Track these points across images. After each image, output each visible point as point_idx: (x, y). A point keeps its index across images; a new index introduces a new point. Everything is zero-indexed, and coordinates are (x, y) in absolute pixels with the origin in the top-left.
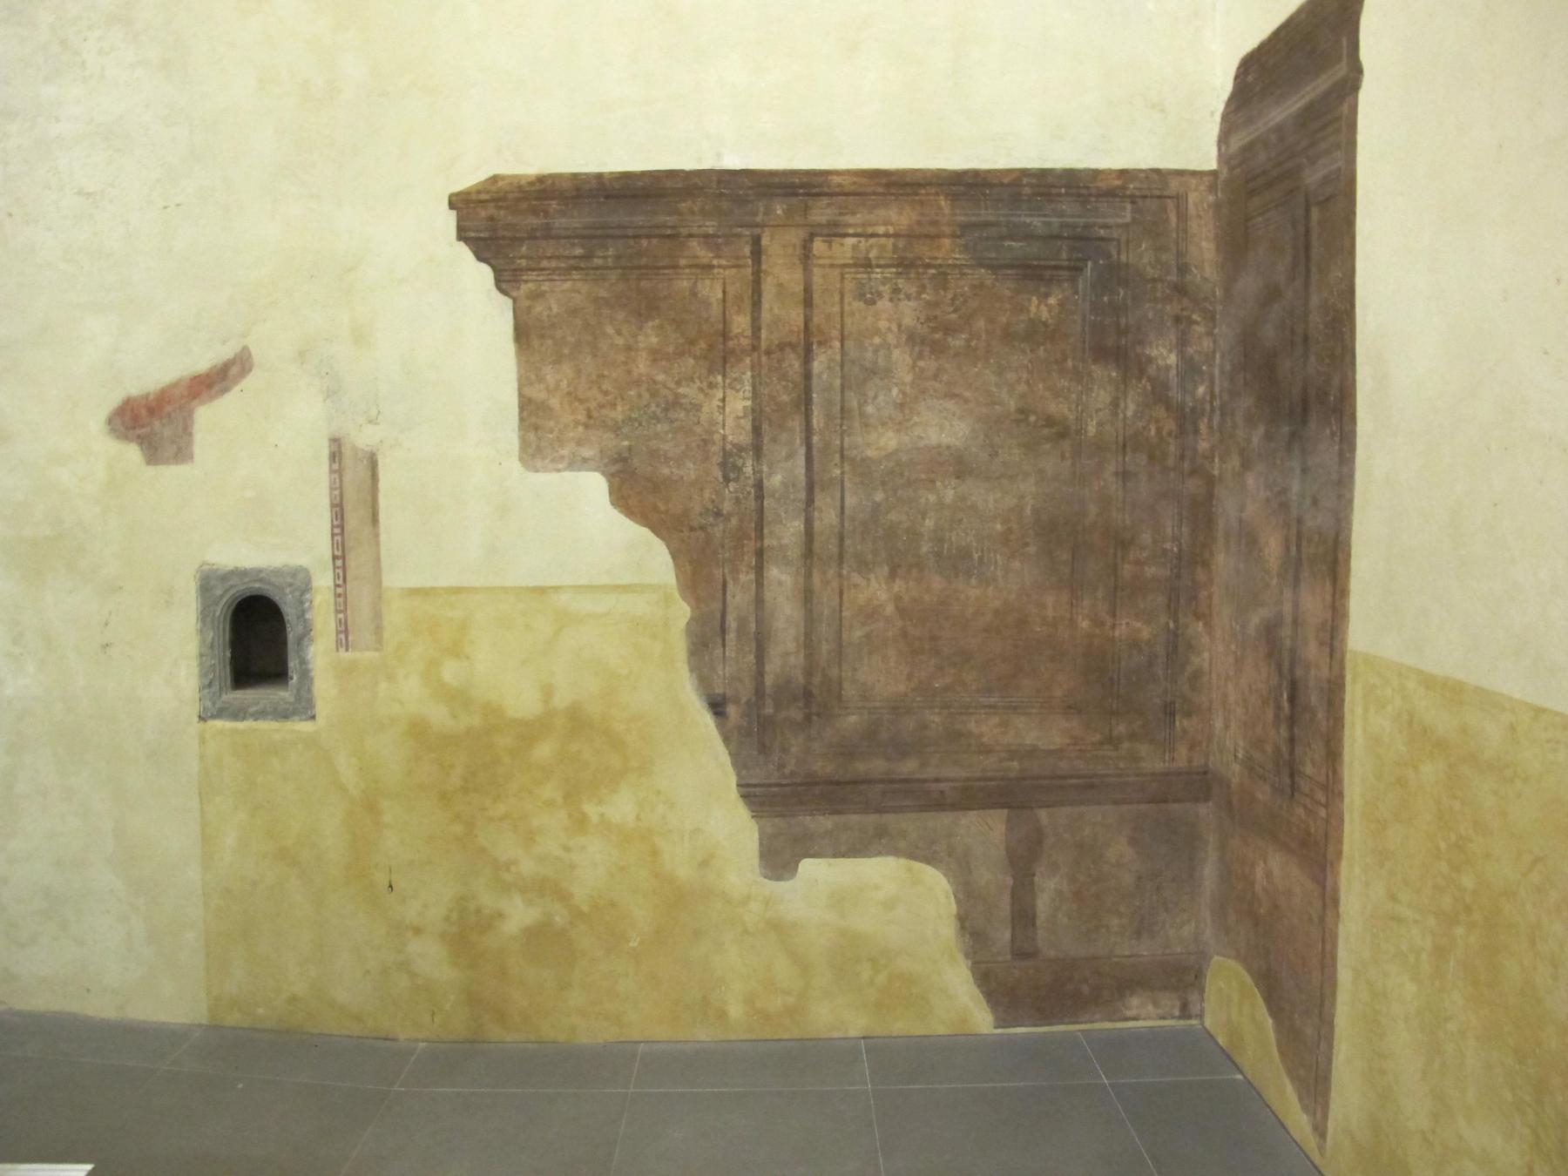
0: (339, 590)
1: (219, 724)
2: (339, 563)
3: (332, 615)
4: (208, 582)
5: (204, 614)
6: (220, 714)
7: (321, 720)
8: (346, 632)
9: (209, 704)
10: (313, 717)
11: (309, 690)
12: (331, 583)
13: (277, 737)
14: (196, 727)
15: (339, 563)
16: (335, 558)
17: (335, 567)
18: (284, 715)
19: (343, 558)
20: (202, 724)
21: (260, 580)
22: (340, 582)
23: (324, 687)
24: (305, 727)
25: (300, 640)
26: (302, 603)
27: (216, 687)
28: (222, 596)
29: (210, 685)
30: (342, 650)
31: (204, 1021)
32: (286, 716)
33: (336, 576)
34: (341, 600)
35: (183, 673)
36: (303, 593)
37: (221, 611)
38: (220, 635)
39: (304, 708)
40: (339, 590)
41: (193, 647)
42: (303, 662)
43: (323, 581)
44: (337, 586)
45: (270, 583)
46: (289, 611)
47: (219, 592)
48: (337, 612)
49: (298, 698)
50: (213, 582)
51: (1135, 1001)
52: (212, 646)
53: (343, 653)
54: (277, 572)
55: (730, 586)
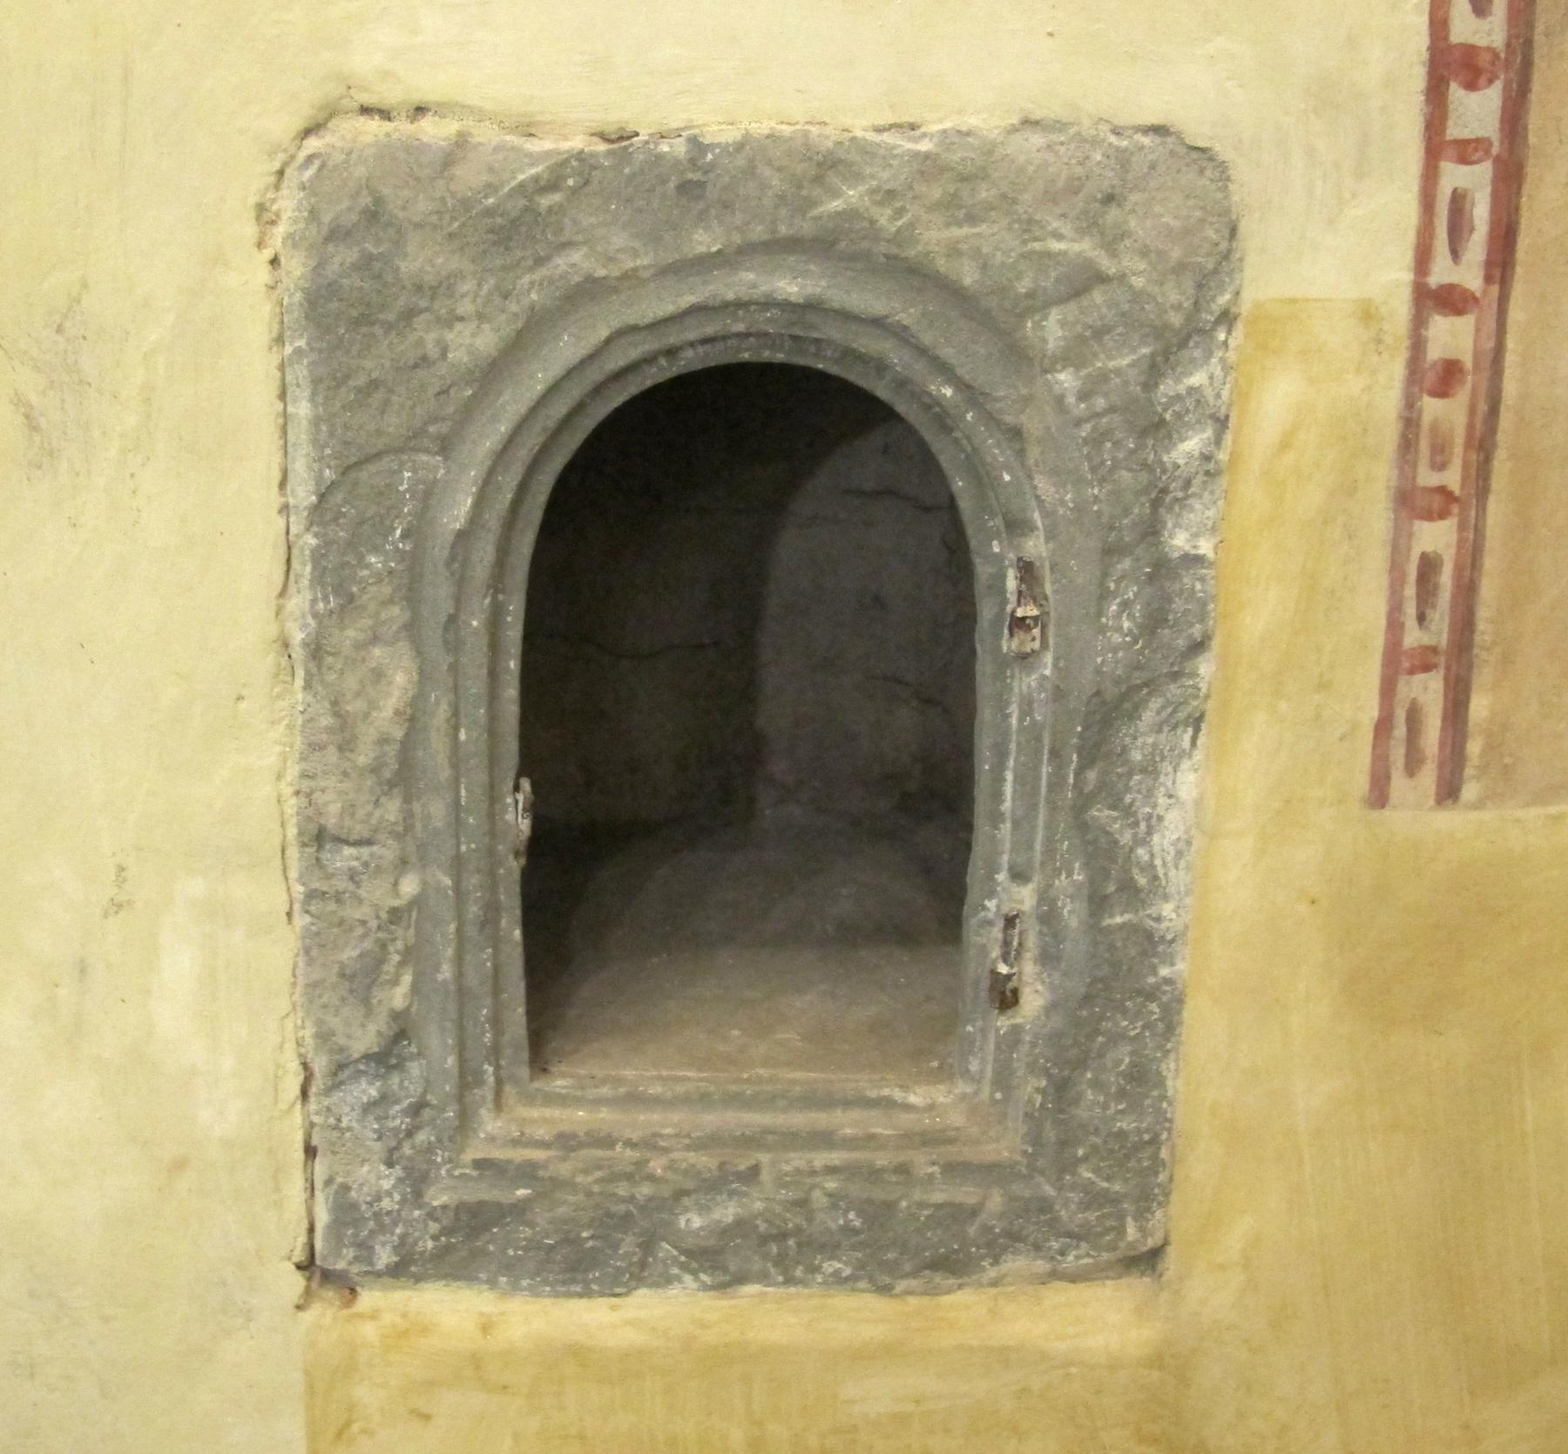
0: (1451, 336)
1: (453, 1310)
2: (1476, 111)
3: (1377, 517)
4: (373, 260)
5: (347, 520)
6: (469, 1242)
7: (1212, 1283)
8: (1458, 663)
9: (376, 1180)
10: (1147, 1260)
11: (1143, 1080)
12: (1392, 280)
13: (875, 1395)
14: (281, 1329)
15: (1476, 111)
16: (1449, 66)
17: (1438, 145)
18: (909, 1240)
19: (1517, 68)
20: (324, 1312)
21: (823, 246)
22: (1469, 274)
23: (1254, 1059)
24: (1089, 1323)
25: (1102, 727)
26: (1156, 429)
27: (437, 1051)
28: (491, 373)
29: (386, 1059)
30: (1413, 792)
31: (376, 1050)
32: (945, 1253)
33: (1440, 221)
34: (1448, 414)
35: (180, 965)
36: (1175, 343)
37: (472, 495)
38: (449, 687)
39: (1089, 1186)
40: (1451, 336)
41: (255, 769)
42: (1115, 879)
43: (1332, 254)
44: (1434, 300)
45: (914, 274)
46: (1034, 527)
47: (471, 342)
48: (1411, 503)
49: (1056, 1136)
50: (421, 259)
51: (331, 1294)
52: (403, 774)
53: (1414, 814)
54: (960, 176)
55: (969, 1154)
